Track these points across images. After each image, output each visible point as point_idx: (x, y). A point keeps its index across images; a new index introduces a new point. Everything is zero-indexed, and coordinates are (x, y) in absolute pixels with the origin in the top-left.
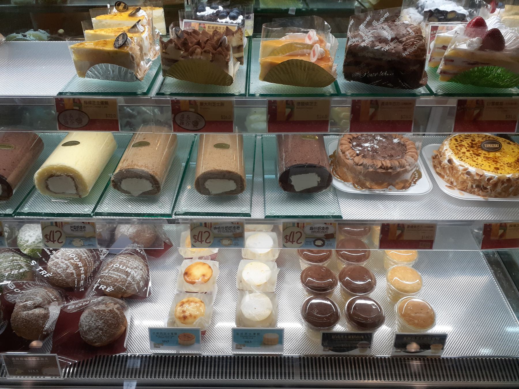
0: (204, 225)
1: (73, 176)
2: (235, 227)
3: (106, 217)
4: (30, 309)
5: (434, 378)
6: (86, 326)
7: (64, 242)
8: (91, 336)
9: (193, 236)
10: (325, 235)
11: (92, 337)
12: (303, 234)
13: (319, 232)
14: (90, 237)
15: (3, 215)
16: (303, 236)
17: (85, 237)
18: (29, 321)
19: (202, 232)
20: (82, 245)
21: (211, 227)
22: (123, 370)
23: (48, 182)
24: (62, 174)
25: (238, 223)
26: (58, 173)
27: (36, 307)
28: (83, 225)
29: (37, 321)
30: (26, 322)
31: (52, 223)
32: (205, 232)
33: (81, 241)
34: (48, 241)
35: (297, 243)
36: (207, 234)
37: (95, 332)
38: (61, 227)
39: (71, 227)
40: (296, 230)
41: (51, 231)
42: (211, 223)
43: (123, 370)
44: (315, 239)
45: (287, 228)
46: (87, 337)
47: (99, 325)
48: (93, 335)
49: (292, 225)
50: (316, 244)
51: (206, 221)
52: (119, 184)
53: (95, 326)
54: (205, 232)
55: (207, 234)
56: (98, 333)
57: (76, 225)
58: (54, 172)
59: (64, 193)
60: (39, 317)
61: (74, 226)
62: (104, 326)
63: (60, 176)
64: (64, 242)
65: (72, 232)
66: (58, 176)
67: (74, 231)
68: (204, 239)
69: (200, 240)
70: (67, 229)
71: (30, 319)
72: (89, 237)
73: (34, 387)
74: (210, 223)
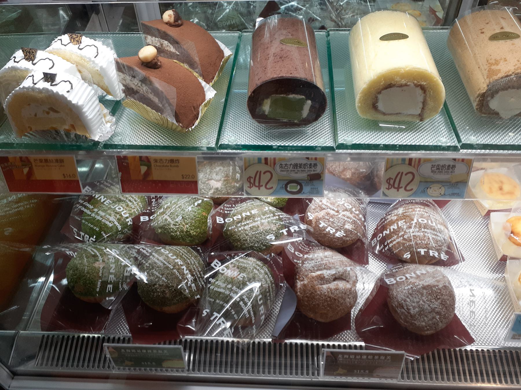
0: (263, 161)
1: (426, 86)
2: (311, 165)
3: (478, 151)
4: (328, 281)
5: (411, 375)
6: (414, 308)
7: (274, 188)
8: (423, 322)
9: (387, 181)
10: (308, 175)
11: (424, 324)
12: (416, 177)
13: (305, 171)
14: (458, 182)
15: (320, 149)
16: (417, 179)
17: (450, 182)
18: (335, 299)
19: (261, 172)
20: (442, 194)
21: (275, 164)
22: (98, 356)
23: (380, 96)
24: (408, 83)
25: (316, 159)
26: (403, 82)
27: (335, 279)
28: (452, 163)
29: (344, 300)
30: (331, 301)
31: (404, 160)
32: (264, 173)
33: (443, 188)
34: (251, 185)
35: (405, 189)
36: (410, 176)
37: (430, 317)
38: (416, 167)
39: (433, 166)
40: (406, 169)
41: (257, 172)
42: (275, 159)
43: (98, 356)
44: (287, 182)
45: (391, 167)
46: (416, 322)
47: (436, 308)
48: (426, 320)
49: (257, 161)
50: (288, 189)
51: (275, 157)
52: (489, 99)
53: (429, 308)
54: (264, 173)
55: (268, 175)
56: (433, 318)
57: (441, 163)
58: (398, 79)
59: (400, 113)
60: (345, 293)
61: (438, 165)
62: (442, 309)
63: (406, 85)
64: (274, 188)
65: (432, 174)
66: (401, 86)
67: (436, 172)
68: (263, 183)
69: (257, 184)
70: (425, 169)
71: (336, 296)
72: (456, 182)
73: (129, 378)
74: (272, 157)
